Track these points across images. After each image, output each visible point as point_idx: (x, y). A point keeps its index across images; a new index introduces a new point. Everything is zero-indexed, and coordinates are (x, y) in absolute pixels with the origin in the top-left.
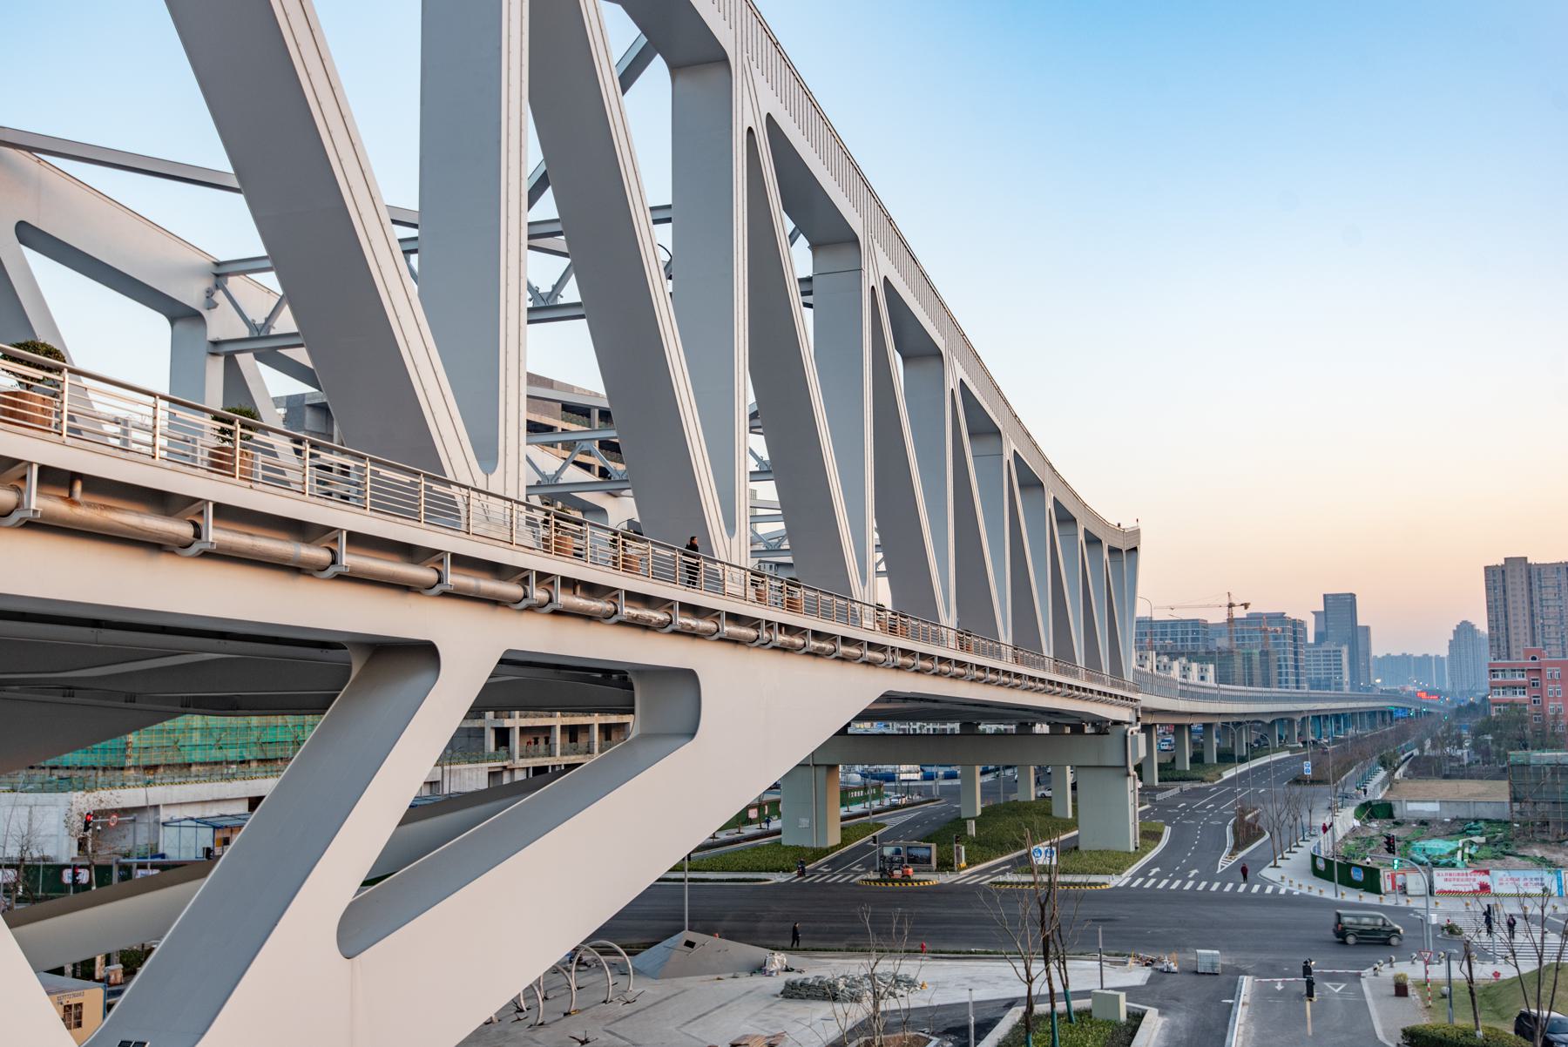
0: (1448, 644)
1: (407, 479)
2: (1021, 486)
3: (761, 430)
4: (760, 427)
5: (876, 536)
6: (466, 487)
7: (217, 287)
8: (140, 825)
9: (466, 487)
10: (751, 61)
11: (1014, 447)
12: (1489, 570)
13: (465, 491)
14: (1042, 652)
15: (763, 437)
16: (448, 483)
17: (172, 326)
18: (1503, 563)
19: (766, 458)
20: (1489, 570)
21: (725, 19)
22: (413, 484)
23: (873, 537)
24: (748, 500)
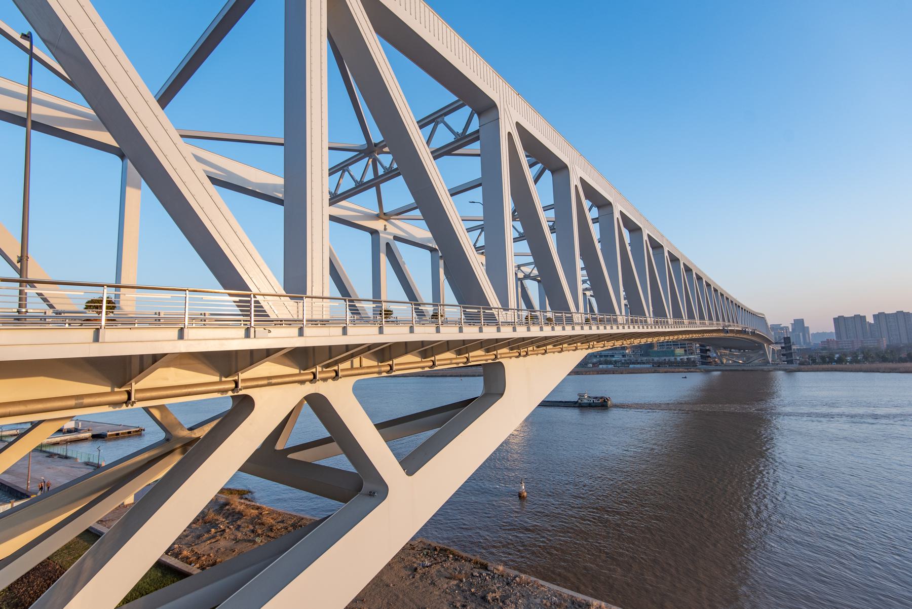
0: (862, 315)
1: (476, 311)
2: (671, 261)
3: (518, 219)
4: (517, 218)
5: (624, 293)
6: (497, 308)
7: (518, 269)
8: (780, 420)
9: (497, 308)
10: (508, 104)
11: (667, 249)
12: (834, 319)
13: (497, 310)
14: (594, 312)
15: (519, 222)
16: (491, 309)
17: (122, 161)
18: (832, 329)
19: (522, 231)
20: (834, 319)
21: (459, 58)
22: (478, 312)
23: (622, 294)
24: (513, 262)
